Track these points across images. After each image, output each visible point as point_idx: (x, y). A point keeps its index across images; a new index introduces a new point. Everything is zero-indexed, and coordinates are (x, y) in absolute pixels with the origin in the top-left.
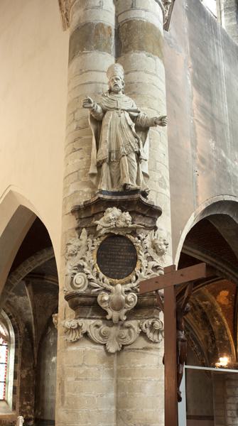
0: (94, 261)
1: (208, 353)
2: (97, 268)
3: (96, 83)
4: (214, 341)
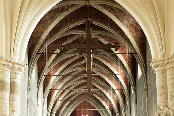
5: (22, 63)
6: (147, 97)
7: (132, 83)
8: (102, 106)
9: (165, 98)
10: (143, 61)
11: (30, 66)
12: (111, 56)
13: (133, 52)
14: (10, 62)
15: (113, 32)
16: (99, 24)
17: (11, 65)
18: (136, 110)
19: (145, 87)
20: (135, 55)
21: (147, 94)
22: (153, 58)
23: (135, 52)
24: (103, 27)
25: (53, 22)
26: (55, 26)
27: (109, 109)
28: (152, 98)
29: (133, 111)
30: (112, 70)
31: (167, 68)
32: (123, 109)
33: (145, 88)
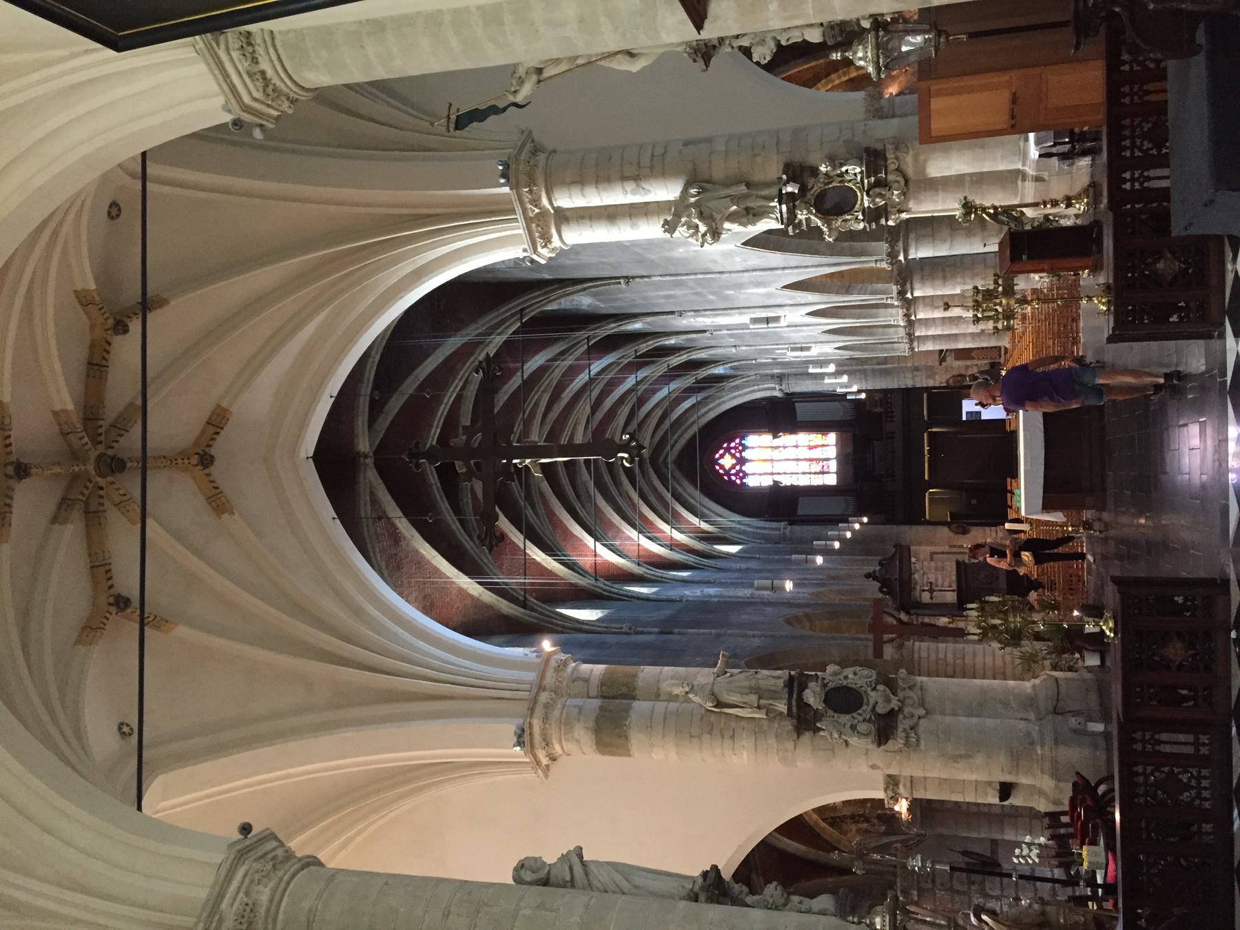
0: (848, 717)
1: (886, 834)
2: (855, 715)
3: (665, 714)
4: (867, 820)
5: (538, 660)
6: (649, 277)
7: (613, 325)
8: (687, 415)
9: (1003, 646)
10: (543, 291)
11: (563, 627)
12: (538, 389)
13: (516, 320)
14: (535, 700)
15: (460, 380)
16: (438, 424)
17: (544, 697)
18: (692, 313)
19: (620, 283)
20: (526, 314)
21: (643, 277)
22: (521, 255)
23: (519, 316)
24: (443, 411)
25: (429, 563)
26: (439, 556)
27: (634, 376)
28: (652, 261)
29: (697, 324)
30: (579, 385)
31: (549, 207)
32: (694, 353)
33: (623, 286)
